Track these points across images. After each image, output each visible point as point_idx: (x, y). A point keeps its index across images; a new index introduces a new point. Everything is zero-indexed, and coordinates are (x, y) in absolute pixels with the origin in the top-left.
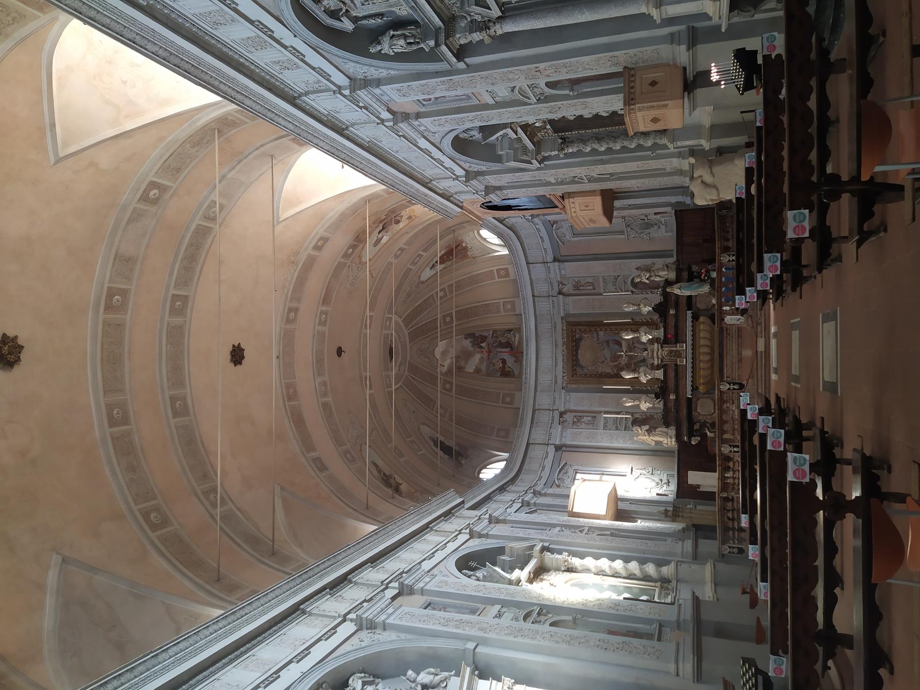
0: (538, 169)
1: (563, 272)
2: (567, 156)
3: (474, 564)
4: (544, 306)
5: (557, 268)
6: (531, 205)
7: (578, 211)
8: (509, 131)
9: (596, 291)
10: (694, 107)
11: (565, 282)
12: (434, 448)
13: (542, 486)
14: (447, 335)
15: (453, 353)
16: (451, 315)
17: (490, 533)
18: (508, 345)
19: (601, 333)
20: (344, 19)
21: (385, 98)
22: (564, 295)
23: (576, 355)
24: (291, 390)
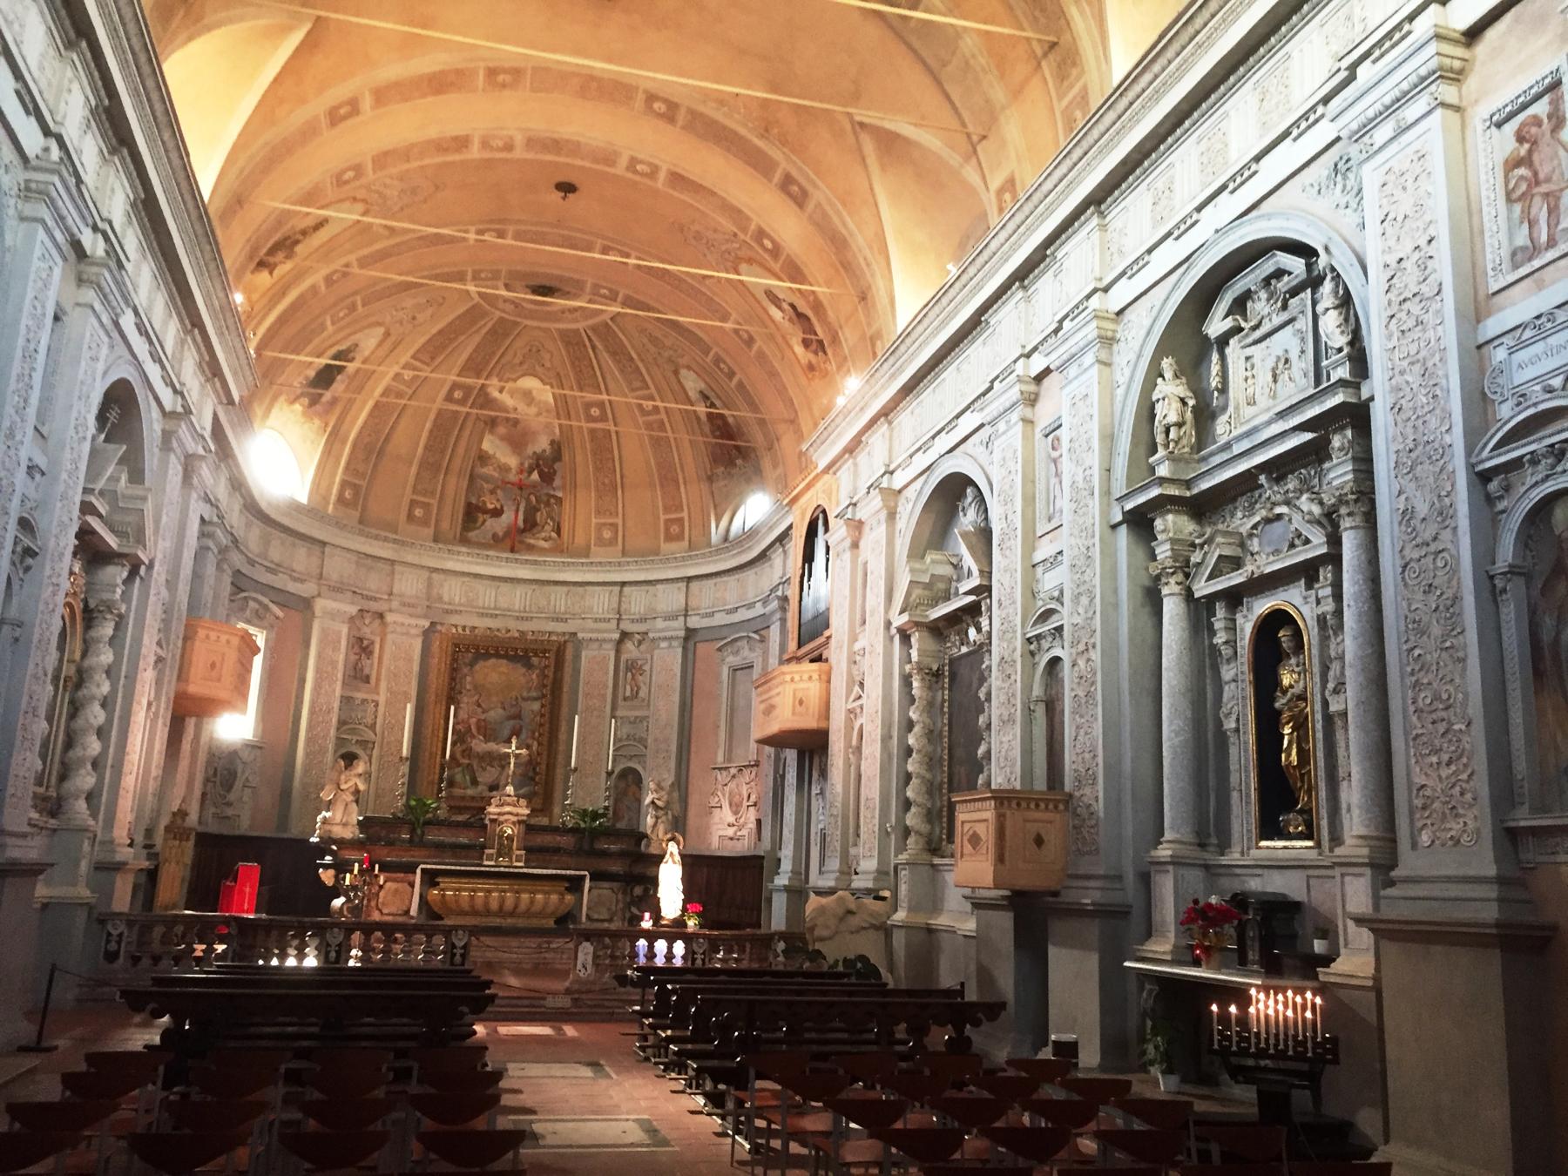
0: (888, 624)
1: (664, 644)
2: (906, 681)
3: (113, 416)
4: (600, 602)
5: (673, 634)
6: (808, 601)
7: (793, 686)
8: (975, 581)
9: (620, 702)
10: (979, 905)
11: (643, 647)
12: (333, 351)
13: (238, 565)
14: (563, 407)
15: (525, 412)
16: (603, 418)
17: (172, 456)
18: (531, 525)
19: (536, 706)
20: (1229, 323)
21: (1073, 370)
22: (620, 642)
23: (497, 656)
24: (508, 78)
